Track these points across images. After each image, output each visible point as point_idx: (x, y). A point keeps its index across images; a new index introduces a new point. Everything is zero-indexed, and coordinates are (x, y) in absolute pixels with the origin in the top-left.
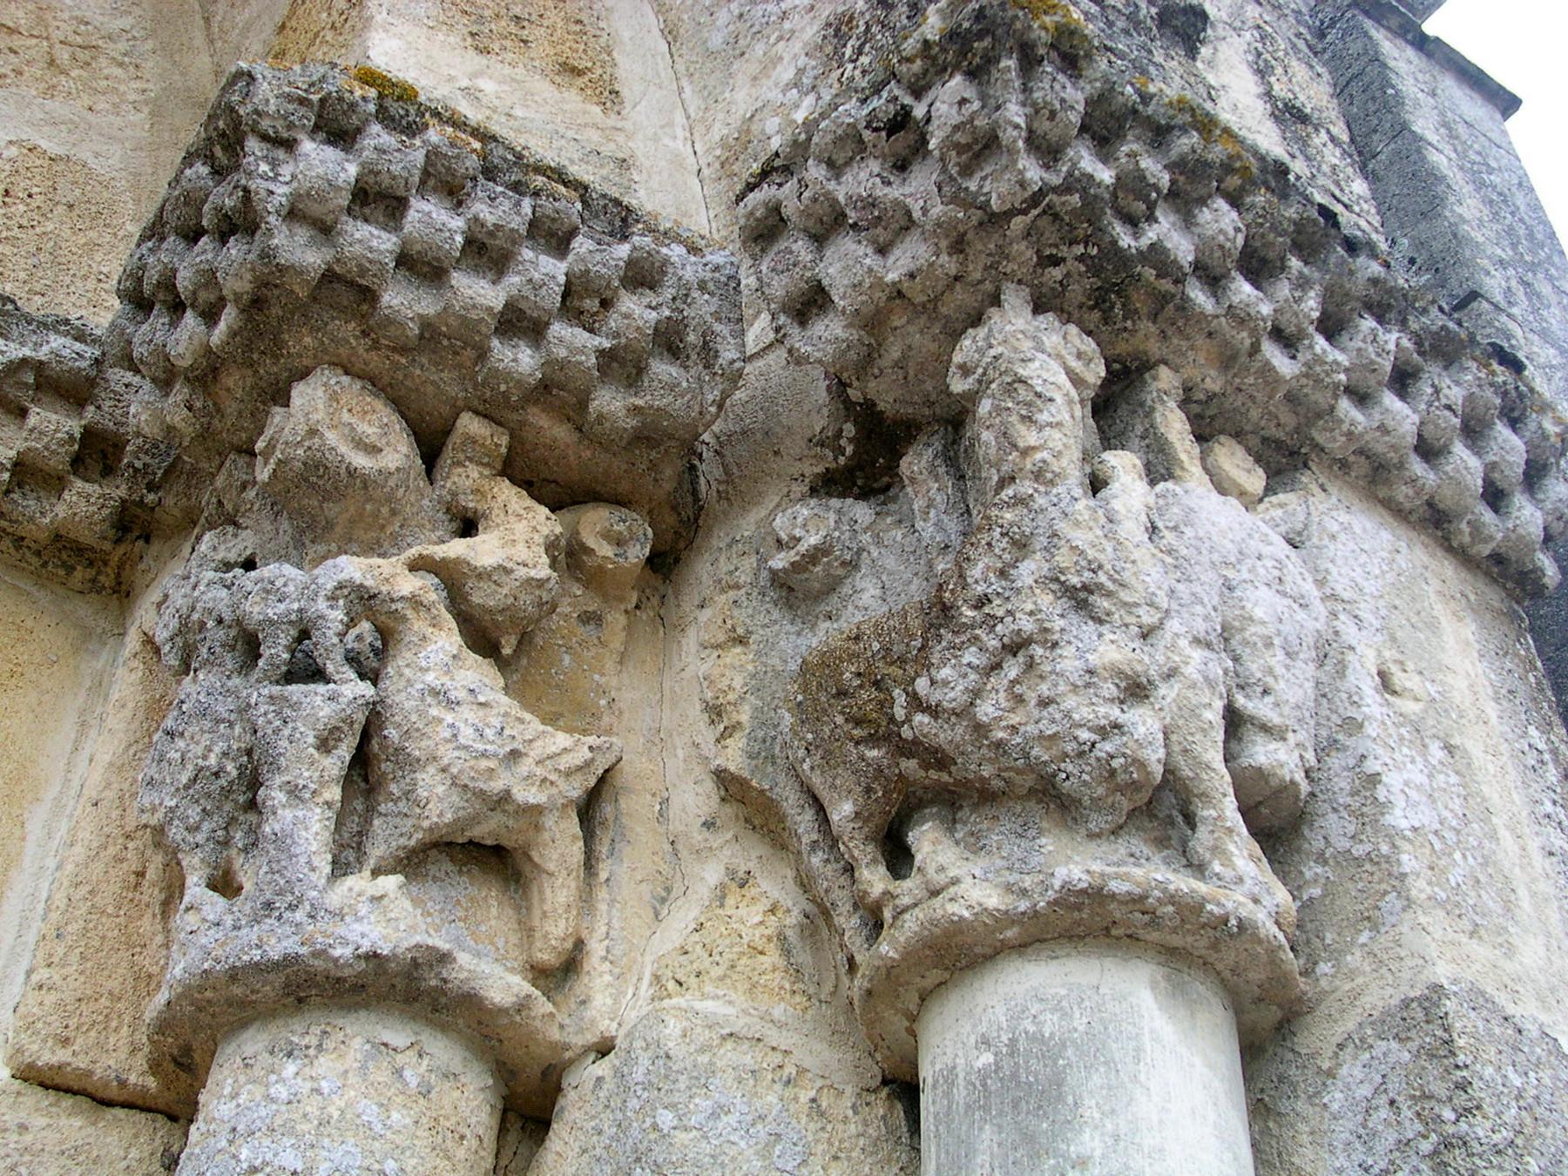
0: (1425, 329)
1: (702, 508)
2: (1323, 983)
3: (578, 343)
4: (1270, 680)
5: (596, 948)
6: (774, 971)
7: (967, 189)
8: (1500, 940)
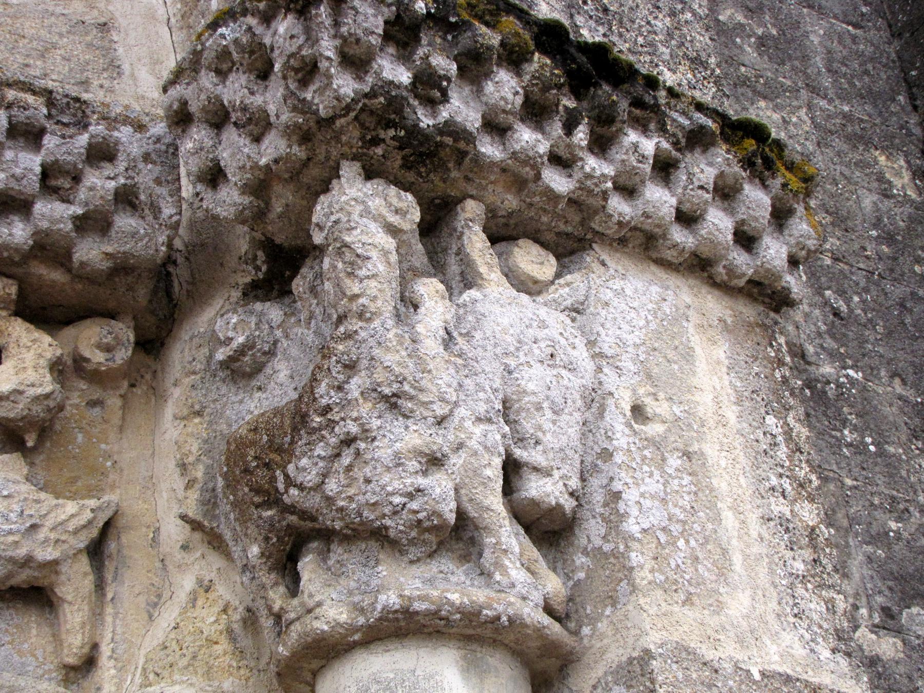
1: (175, 305)
2: (585, 641)
3: (57, 215)
4: (540, 434)
5: (105, 650)
6: (225, 655)
7: (304, 99)
8: (711, 601)
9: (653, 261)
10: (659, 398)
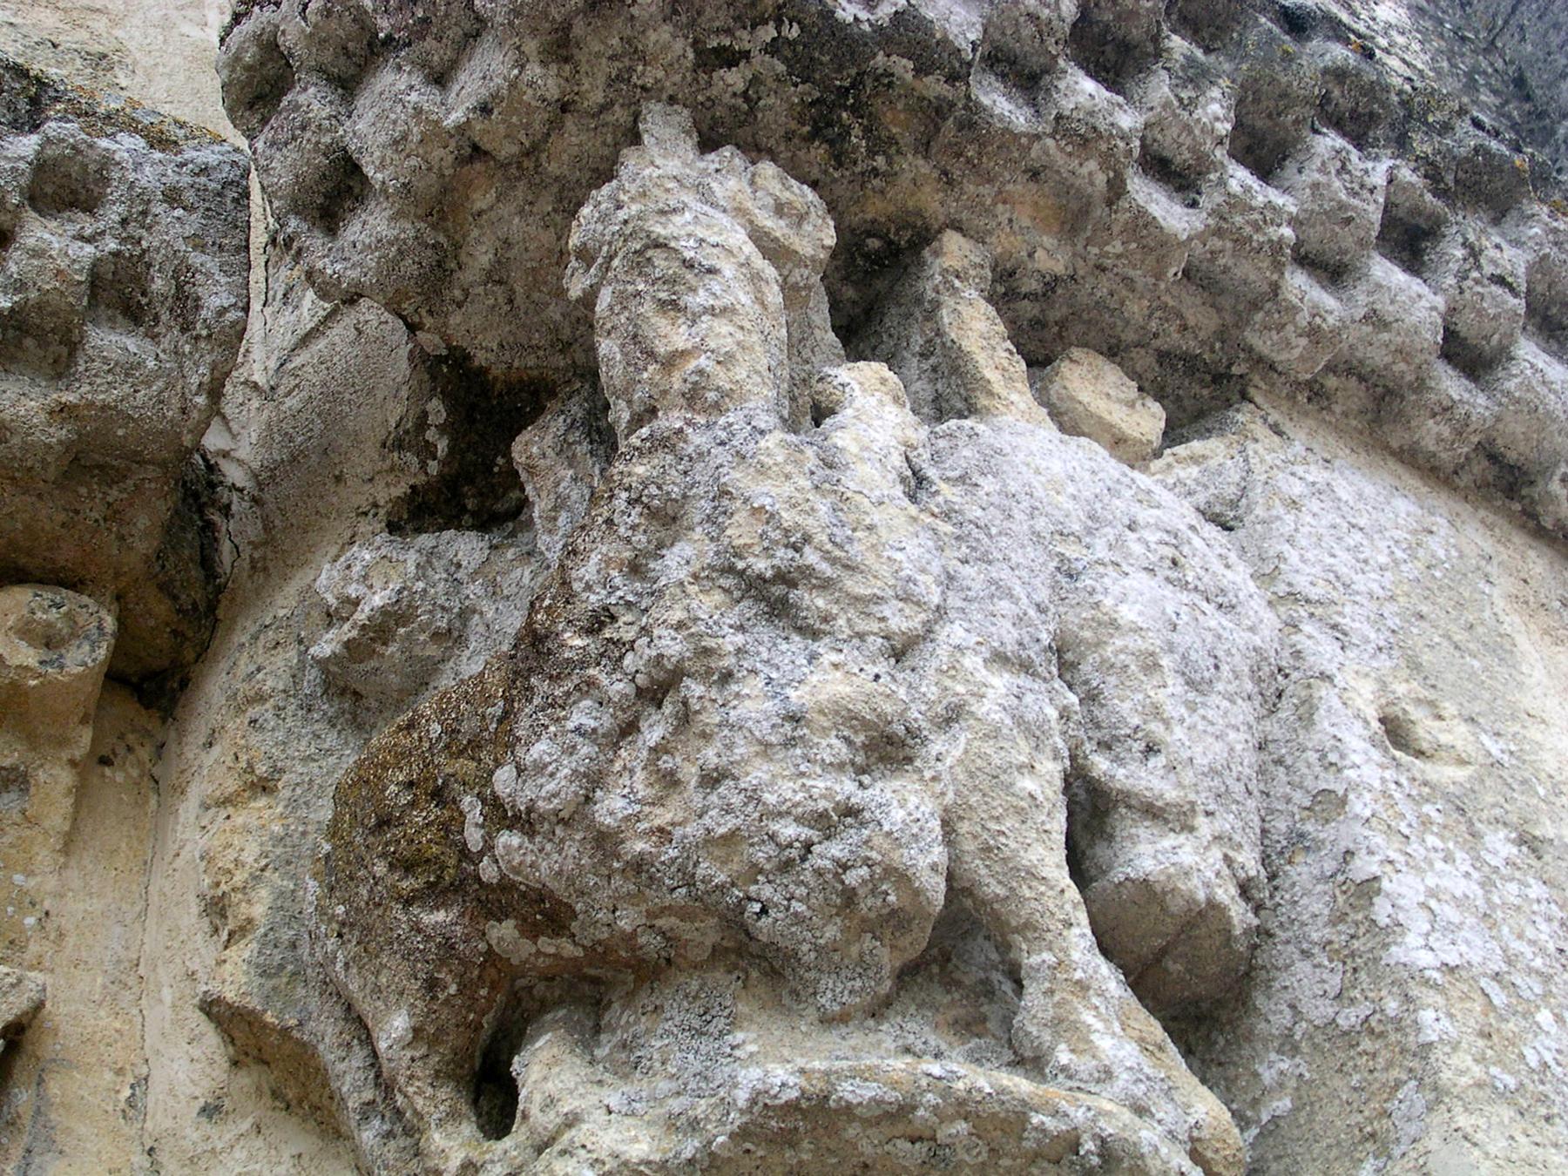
0: (1447, 154)
1: (220, 590)
4: (1156, 727)
9: (1393, 453)
10: (1445, 714)
